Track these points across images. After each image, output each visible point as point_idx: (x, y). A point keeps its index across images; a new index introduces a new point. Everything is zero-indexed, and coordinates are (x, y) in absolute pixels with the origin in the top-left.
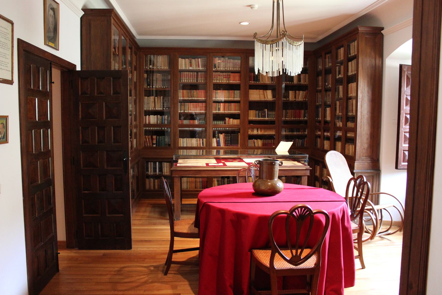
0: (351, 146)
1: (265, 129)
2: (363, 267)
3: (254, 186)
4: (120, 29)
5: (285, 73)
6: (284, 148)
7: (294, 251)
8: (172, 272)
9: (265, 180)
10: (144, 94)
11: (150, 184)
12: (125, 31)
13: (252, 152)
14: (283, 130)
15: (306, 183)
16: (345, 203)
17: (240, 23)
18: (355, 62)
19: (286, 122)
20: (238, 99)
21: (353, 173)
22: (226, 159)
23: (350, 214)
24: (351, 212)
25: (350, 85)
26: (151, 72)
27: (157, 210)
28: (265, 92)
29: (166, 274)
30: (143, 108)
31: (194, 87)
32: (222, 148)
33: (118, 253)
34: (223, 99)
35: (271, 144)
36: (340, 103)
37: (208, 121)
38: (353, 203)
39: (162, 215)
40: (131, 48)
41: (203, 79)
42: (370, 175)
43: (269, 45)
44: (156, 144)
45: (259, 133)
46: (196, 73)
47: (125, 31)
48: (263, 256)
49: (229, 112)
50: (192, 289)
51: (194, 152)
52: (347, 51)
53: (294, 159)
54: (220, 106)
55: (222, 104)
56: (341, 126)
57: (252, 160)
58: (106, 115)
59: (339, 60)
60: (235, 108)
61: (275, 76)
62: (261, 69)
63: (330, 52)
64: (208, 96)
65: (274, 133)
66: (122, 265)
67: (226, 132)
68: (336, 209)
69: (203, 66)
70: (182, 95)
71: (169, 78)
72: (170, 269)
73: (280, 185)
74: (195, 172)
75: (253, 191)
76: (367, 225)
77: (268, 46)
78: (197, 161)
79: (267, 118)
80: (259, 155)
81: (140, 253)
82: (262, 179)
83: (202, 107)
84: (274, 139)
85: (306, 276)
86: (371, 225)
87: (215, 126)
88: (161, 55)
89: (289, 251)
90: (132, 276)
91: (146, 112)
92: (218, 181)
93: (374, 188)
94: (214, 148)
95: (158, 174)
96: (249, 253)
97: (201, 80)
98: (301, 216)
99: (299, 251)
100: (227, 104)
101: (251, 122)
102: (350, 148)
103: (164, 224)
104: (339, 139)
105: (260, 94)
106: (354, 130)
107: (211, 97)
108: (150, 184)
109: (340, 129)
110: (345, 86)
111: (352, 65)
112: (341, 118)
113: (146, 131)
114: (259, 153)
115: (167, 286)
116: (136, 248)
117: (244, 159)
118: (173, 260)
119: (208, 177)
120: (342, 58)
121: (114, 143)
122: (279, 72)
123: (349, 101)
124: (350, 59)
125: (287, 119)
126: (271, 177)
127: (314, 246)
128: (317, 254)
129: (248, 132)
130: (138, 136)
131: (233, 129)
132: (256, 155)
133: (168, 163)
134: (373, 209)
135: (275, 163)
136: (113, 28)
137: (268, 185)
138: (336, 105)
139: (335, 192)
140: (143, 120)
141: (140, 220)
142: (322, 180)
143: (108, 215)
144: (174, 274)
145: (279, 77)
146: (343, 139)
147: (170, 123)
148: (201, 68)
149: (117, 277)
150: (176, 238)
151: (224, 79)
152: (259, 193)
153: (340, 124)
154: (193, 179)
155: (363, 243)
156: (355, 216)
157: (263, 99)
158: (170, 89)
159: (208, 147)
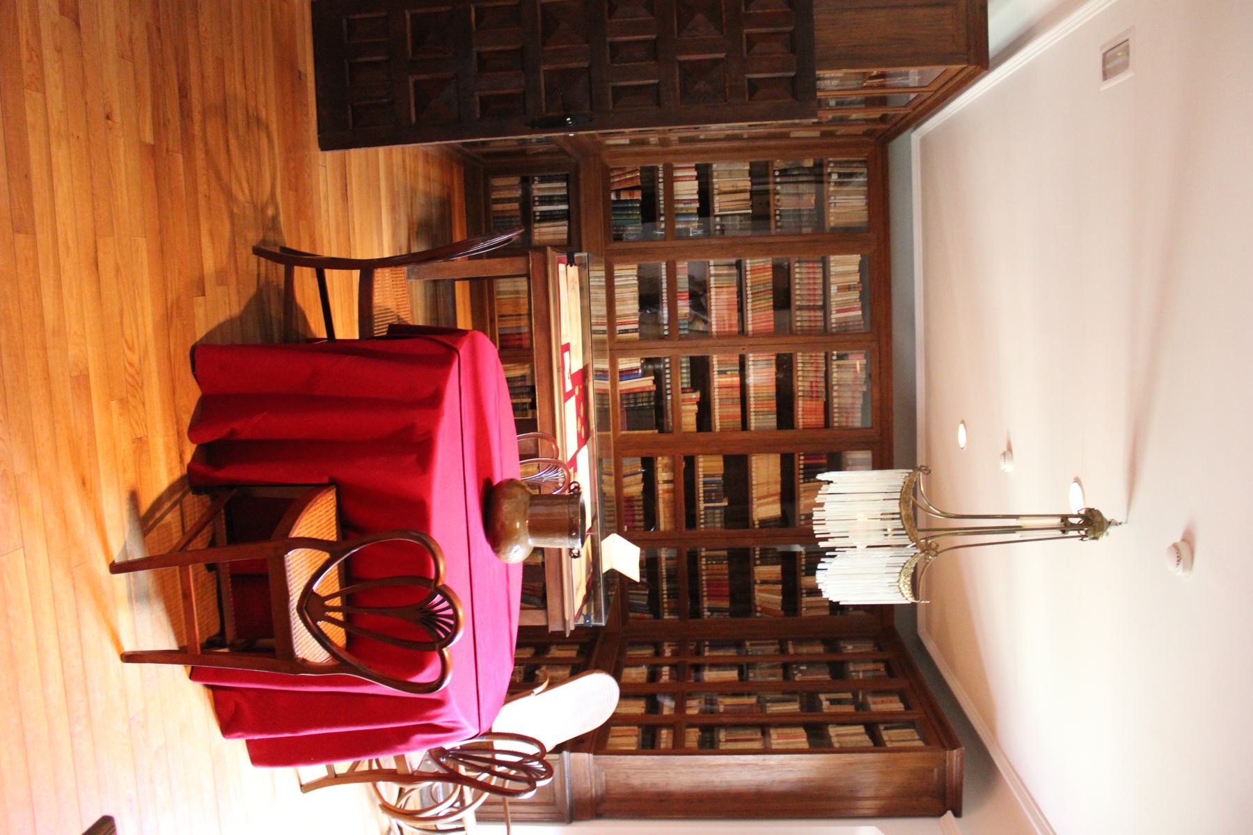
0: (634, 740)
1: (674, 504)
2: (305, 788)
3: (511, 483)
4: (934, 88)
5: (822, 553)
6: (622, 556)
7: (337, 602)
8: (263, 269)
9: (529, 511)
10: (753, 160)
11: (506, 189)
12: (929, 102)
13: (605, 470)
14: (672, 553)
15: (528, 622)
16: (476, 732)
17: (963, 422)
18: (865, 744)
19: (693, 558)
20: (753, 423)
21: (559, 749)
22: (583, 399)
23: (447, 746)
24: (453, 749)
25: (801, 731)
26: (818, 176)
27: (435, 213)
28: (777, 498)
29: (258, 251)
30: (718, 159)
31: (782, 299)
32: (614, 385)
33: (307, 115)
34: (751, 380)
35: (634, 521)
36: (752, 705)
37: (687, 343)
38: (479, 754)
39: (421, 228)
40: (883, 119)
41: (806, 324)
42: (558, 795)
43: (897, 510)
44: (619, 201)
45: (662, 488)
46: (820, 303)
47: (929, 102)
48: (318, 519)
49: (717, 401)
50: (220, 326)
51: (599, 309)
52: (892, 721)
53: (591, 586)
54: (732, 376)
55: (736, 380)
56: (689, 712)
57: (583, 477)
58: (689, 61)
59: (870, 699)
60: (728, 417)
61: (815, 528)
62: (831, 488)
63: (890, 673)
64: (761, 340)
65: (662, 527)
66: (274, 127)
67: (659, 394)
68: (457, 710)
69: (839, 322)
70: (759, 268)
71: (805, 230)
72: (270, 263)
73: (517, 554)
74: (544, 317)
75: (497, 479)
76: (421, 792)
77: (894, 507)
78: (574, 319)
79: (702, 505)
80: (601, 490)
81: (310, 176)
82: (531, 505)
83: (731, 326)
84: (647, 528)
85: (272, 636)
86: (422, 804)
87: (675, 364)
88: (868, 204)
89: (336, 588)
90: (245, 159)
91: (706, 170)
92: (523, 377)
93: (522, 808)
94: (613, 364)
95: (535, 209)
96: (325, 480)
97: (801, 319)
98: (431, 618)
99: (339, 616)
100: (737, 393)
101: (690, 462)
102: (628, 738)
103: (394, 235)
104: (654, 707)
105: (768, 483)
106: (679, 748)
107: (757, 348)
108: (506, 189)
109: (680, 707)
110: (798, 719)
111: (855, 734)
112: (712, 712)
113: (654, 170)
114: (606, 488)
115: (225, 257)
116: (324, 164)
117: (585, 448)
118: (296, 268)
119: (531, 348)
120: (874, 708)
121: (614, 88)
122: (825, 539)
123: (758, 729)
124: (872, 729)
125: (704, 561)
126: (537, 529)
127: (360, 651)
128: (331, 663)
129: (662, 455)
130: (637, 149)
131: (670, 413)
132: (598, 481)
133: (565, 236)
134: (463, 807)
135: (576, 537)
136: (938, 70)
137: (513, 521)
138: (749, 695)
139: (507, 701)
140: (684, 161)
141: (404, 167)
142: (538, 667)
143: (411, 80)
144: (259, 275)
145: (809, 537)
146: (652, 719)
147: (682, 236)
148: (834, 317)
149: (241, 116)
150: (356, 274)
151: (807, 384)
152: (491, 497)
153: (694, 707)
154: (524, 310)
155: (370, 784)
156: (443, 760)
157: (755, 492)
158: (773, 232)
159: (618, 346)
